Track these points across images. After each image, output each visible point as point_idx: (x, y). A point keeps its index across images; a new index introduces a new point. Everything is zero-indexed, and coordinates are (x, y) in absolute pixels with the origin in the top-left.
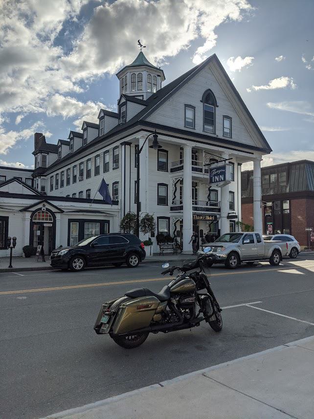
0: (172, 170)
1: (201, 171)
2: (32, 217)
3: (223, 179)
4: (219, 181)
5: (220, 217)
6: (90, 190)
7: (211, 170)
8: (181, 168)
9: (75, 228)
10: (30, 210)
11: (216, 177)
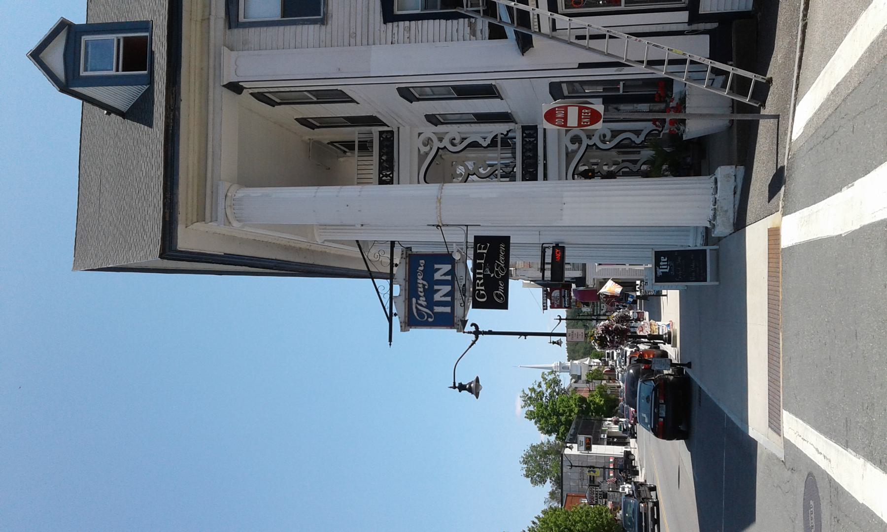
11: (437, 297)
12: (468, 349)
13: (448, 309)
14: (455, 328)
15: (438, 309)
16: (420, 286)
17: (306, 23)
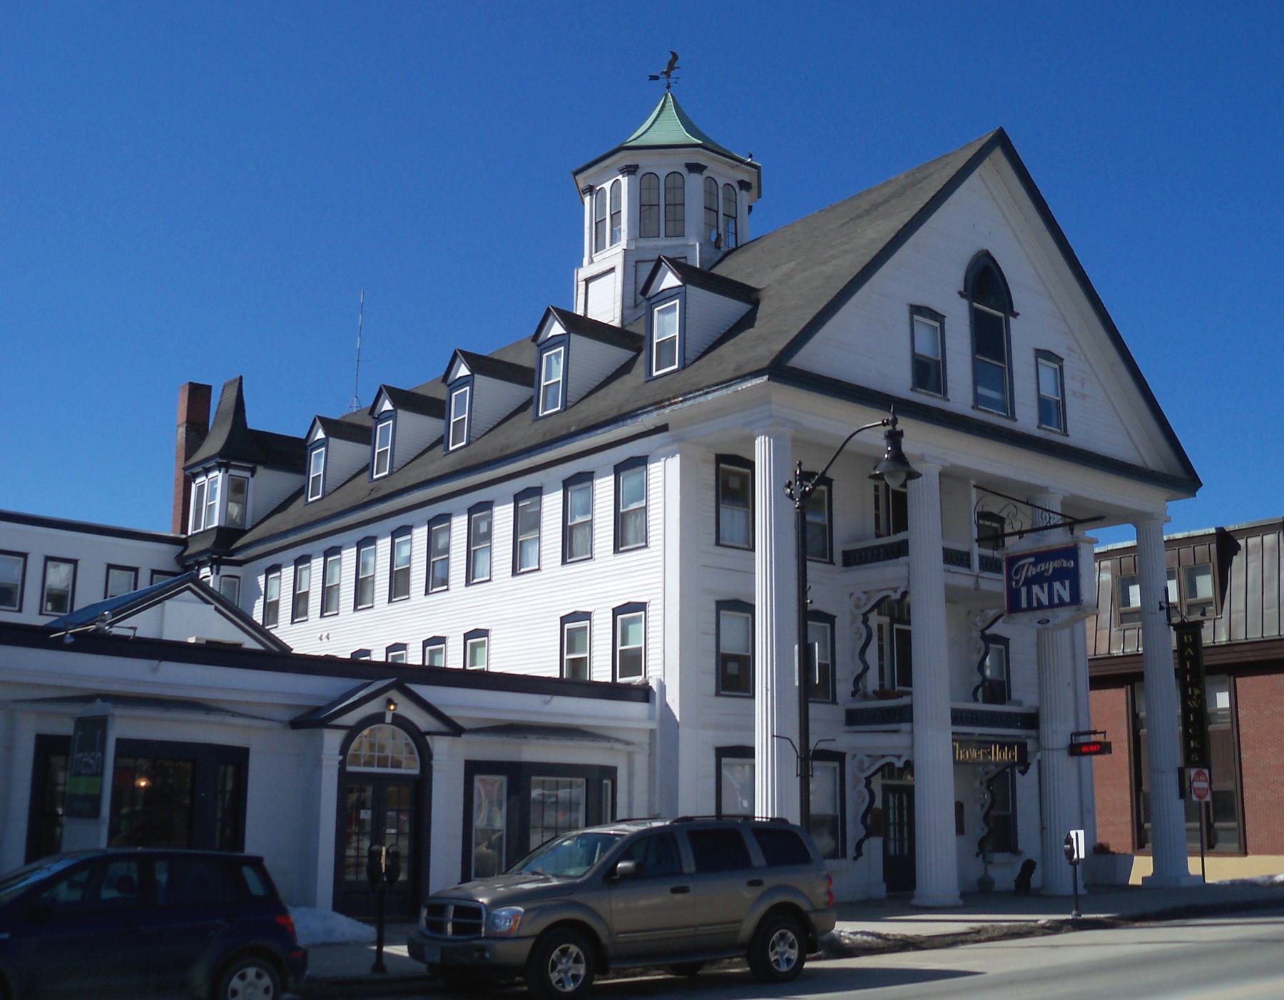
0: (853, 559)
1: (968, 565)
2: (344, 749)
3: (1067, 598)
4: (1051, 605)
5: (1039, 748)
6: (485, 633)
7: (1012, 560)
8: (901, 550)
9: (490, 788)
10: (339, 721)
11: (1036, 588)
12: (125, 628)
13: (1024, 604)
14: (628, 627)
15: (1024, 590)
16: (1047, 567)
17: (517, 861)
